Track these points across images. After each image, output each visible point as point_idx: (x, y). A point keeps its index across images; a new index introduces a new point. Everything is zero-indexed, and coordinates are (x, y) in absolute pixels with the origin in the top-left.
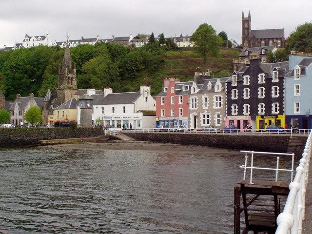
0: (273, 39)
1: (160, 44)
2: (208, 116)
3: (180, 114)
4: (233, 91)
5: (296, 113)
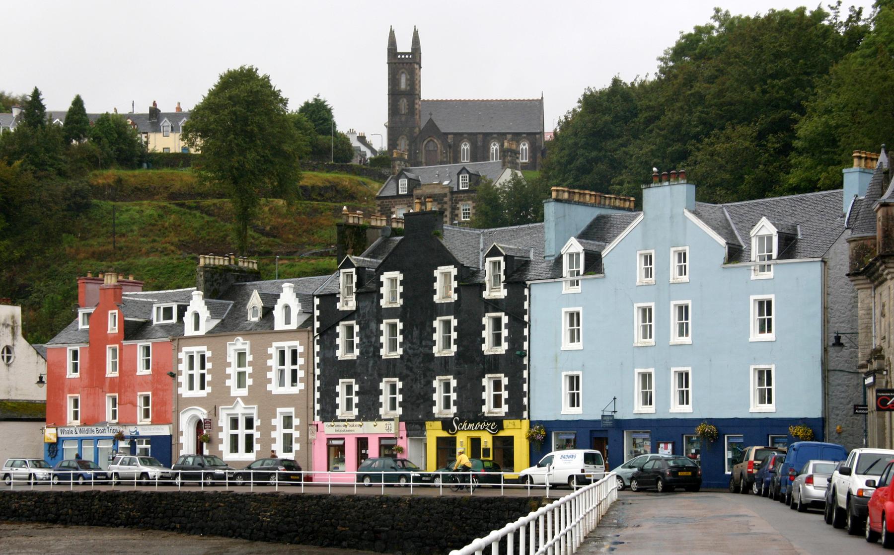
0: (501, 136)
1: (68, 141)
2: (249, 423)
3: (140, 413)
4: (340, 329)
5: (568, 412)
